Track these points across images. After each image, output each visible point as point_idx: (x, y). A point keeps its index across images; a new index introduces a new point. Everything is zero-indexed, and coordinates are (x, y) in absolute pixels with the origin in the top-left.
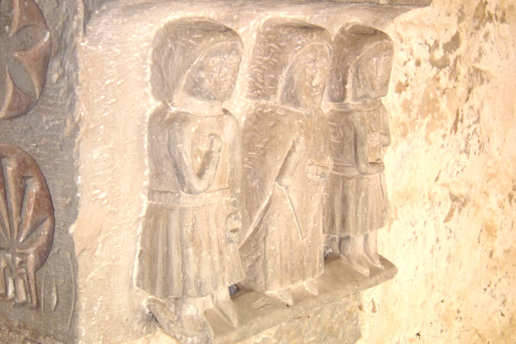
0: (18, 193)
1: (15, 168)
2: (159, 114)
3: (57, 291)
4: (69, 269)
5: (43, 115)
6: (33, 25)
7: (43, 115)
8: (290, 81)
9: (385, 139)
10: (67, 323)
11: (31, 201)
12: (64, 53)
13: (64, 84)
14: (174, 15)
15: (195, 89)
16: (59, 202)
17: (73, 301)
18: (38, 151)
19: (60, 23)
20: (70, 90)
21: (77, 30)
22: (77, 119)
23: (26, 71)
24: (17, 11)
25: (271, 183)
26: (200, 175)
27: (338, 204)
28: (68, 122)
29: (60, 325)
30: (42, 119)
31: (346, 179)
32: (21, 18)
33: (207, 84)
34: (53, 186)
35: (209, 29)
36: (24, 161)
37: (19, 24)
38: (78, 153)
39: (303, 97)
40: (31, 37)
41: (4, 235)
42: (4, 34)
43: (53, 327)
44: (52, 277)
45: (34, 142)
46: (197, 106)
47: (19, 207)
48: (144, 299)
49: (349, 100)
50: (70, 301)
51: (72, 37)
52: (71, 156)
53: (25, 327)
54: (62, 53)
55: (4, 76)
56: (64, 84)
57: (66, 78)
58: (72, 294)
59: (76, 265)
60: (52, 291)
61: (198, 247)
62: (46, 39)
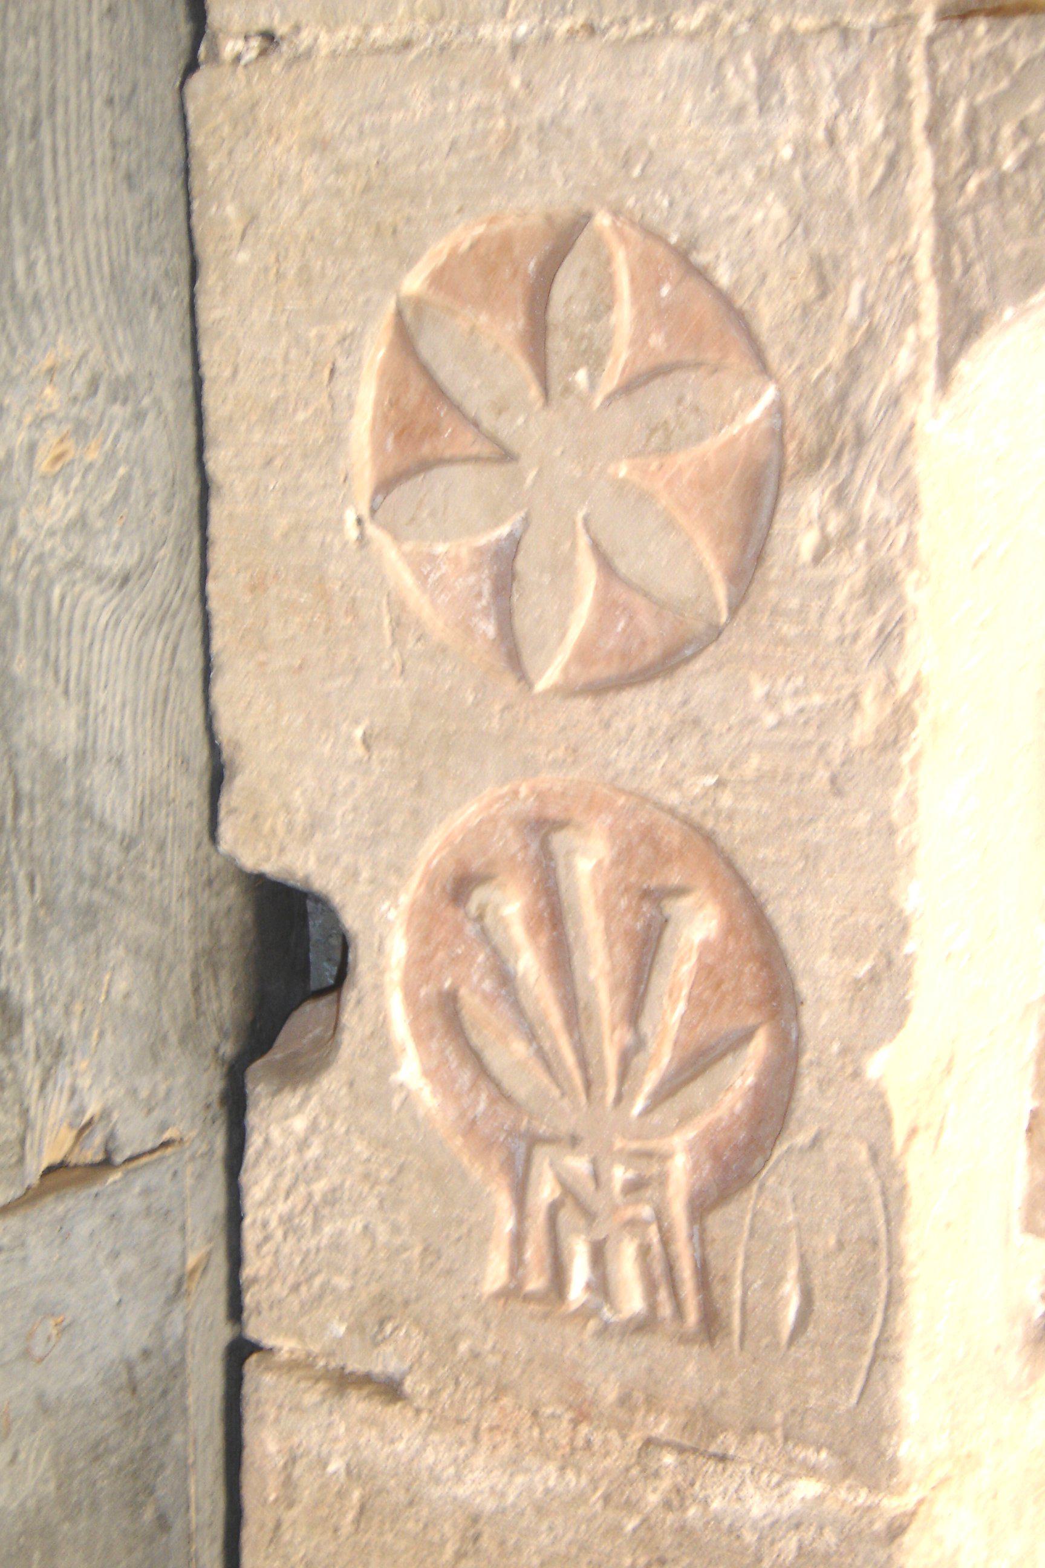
0: (618, 948)
1: (607, 862)
3: (804, 1274)
4: (866, 1199)
5: (754, 678)
6: (698, 365)
7: (754, 678)
10: (850, 1382)
12: (855, 461)
13: (850, 570)
16: (822, 973)
17: (881, 1307)
18: (726, 800)
19: (834, 356)
20: (881, 583)
21: (912, 378)
22: (904, 687)
23: (670, 524)
24: (623, 315)
28: (868, 699)
29: (815, 1392)
30: (748, 690)
32: (639, 340)
34: (798, 919)
36: (648, 834)
37: (632, 360)
38: (911, 801)
40: (696, 409)
41: (555, 1093)
42: (570, 400)
43: (783, 1399)
44: (787, 1229)
45: (706, 770)
47: (623, 997)
50: (863, 1312)
51: (894, 401)
52: (886, 812)
53: (652, 1403)
54: (846, 458)
55: (567, 546)
56: (850, 569)
57: (860, 546)
58: (877, 1285)
59: (896, 1184)
60: (782, 1278)
62: (755, 413)
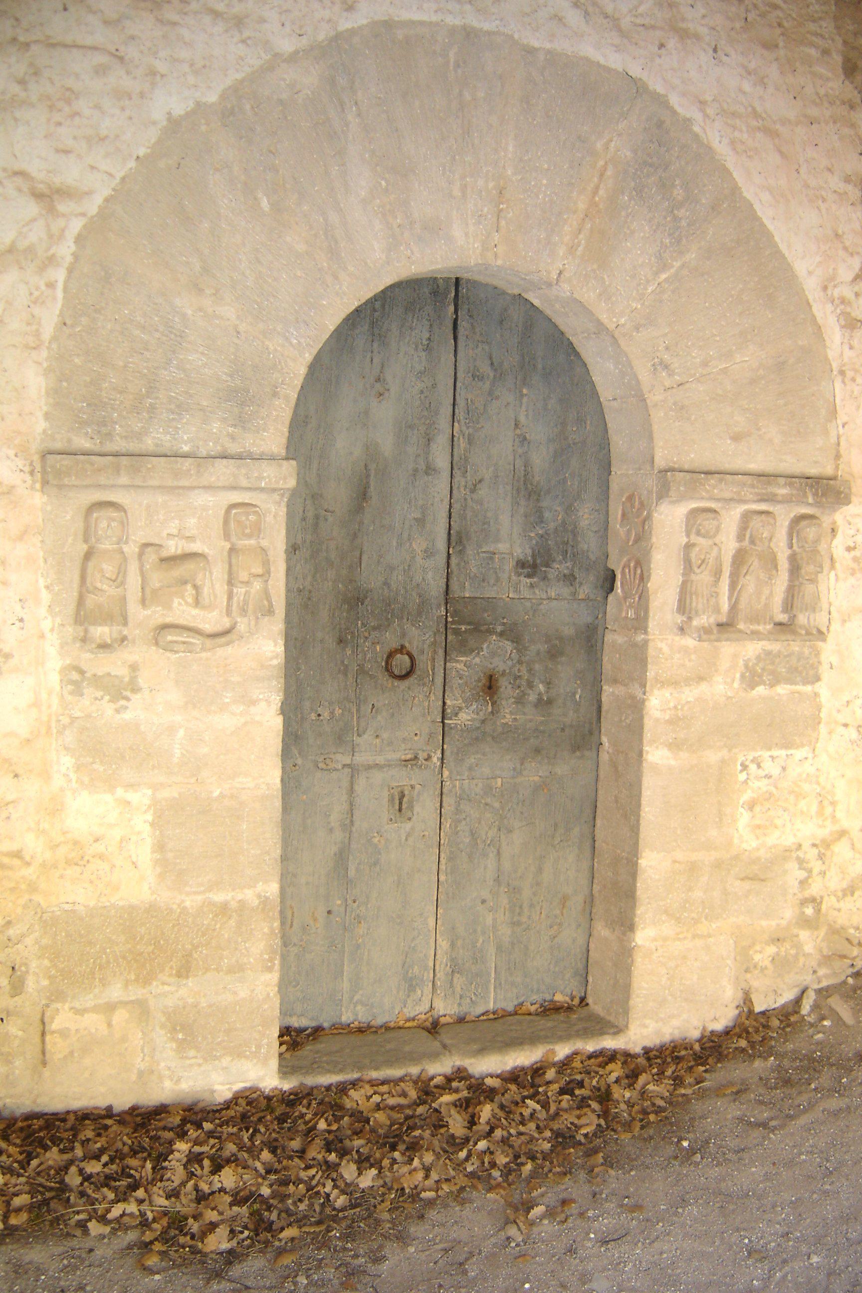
2: (687, 543)
8: (751, 536)
9: (819, 569)
11: (638, 576)
14: (694, 505)
15: (698, 533)
16: (645, 576)
25: (741, 578)
26: (699, 567)
27: (790, 598)
31: (794, 586)
33: (703, 531)
35: (812, 517)
39: (758, 542)
46: (701, 541)
48: (679, 619)
49: (795, 547)
61: (697, 596)
